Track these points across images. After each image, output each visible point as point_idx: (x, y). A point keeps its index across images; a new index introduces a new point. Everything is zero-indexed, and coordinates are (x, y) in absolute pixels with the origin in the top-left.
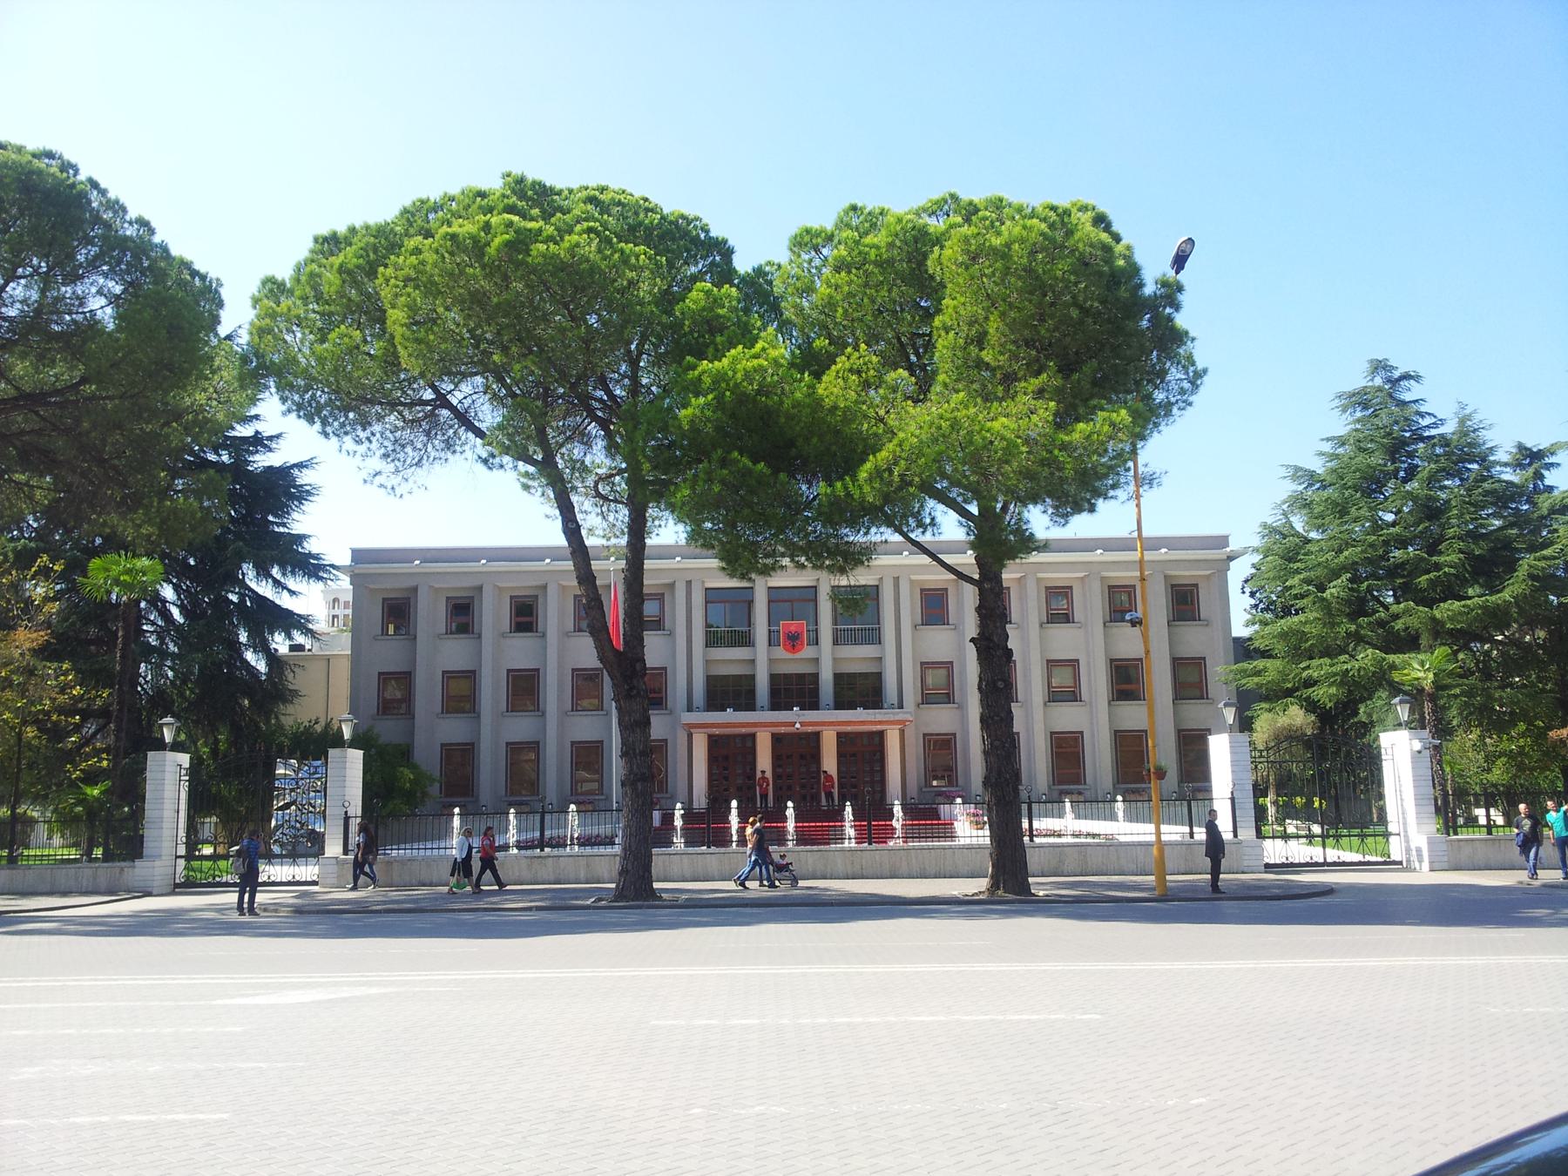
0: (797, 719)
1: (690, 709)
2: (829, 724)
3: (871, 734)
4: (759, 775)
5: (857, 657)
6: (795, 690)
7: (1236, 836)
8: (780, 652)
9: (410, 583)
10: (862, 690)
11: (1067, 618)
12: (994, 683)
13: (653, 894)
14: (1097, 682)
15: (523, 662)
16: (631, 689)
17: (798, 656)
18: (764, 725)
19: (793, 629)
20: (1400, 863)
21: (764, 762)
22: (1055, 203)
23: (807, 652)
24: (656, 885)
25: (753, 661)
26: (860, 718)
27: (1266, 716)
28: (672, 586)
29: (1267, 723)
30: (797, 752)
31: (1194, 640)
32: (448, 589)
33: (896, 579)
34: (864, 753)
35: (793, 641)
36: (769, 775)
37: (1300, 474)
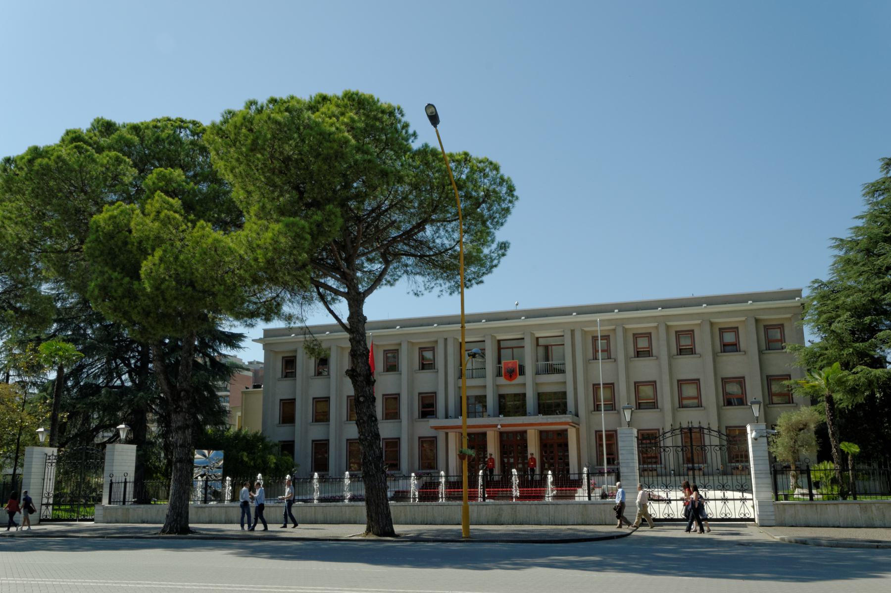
0: (514, 421)
1: (447, 417)
2: (532, 425)
3: (515, 433)
4: (529, 456)
5: (550, 383)
6: (510, 405)
7: (590, 499)
8: (502, 381)
9: (292, 347)
10: (552, 404)
11: (691, 351)
12: (358, 398)
13: (188, 530)
14: (710, 394)
15: (427, 388)
16: (177, 408)
17: (514, 382)
18: (493, 425)
19: (510, 365)
20: (753, 520)
21: (533, 449)
22: (277, 96)
23: (519, 379)
24: (190, 525)
25: (485, 387)
26: (553, 422)
27: (784, 415)
28: (436, 342)
29: (785, 418)
30: (513, 444)
31: (778, 363)
32: (283, 352)
33: (573, 331)
34: (555, 447)
35: (511, 374)
36: (537, 456)
37: (841, 243)
